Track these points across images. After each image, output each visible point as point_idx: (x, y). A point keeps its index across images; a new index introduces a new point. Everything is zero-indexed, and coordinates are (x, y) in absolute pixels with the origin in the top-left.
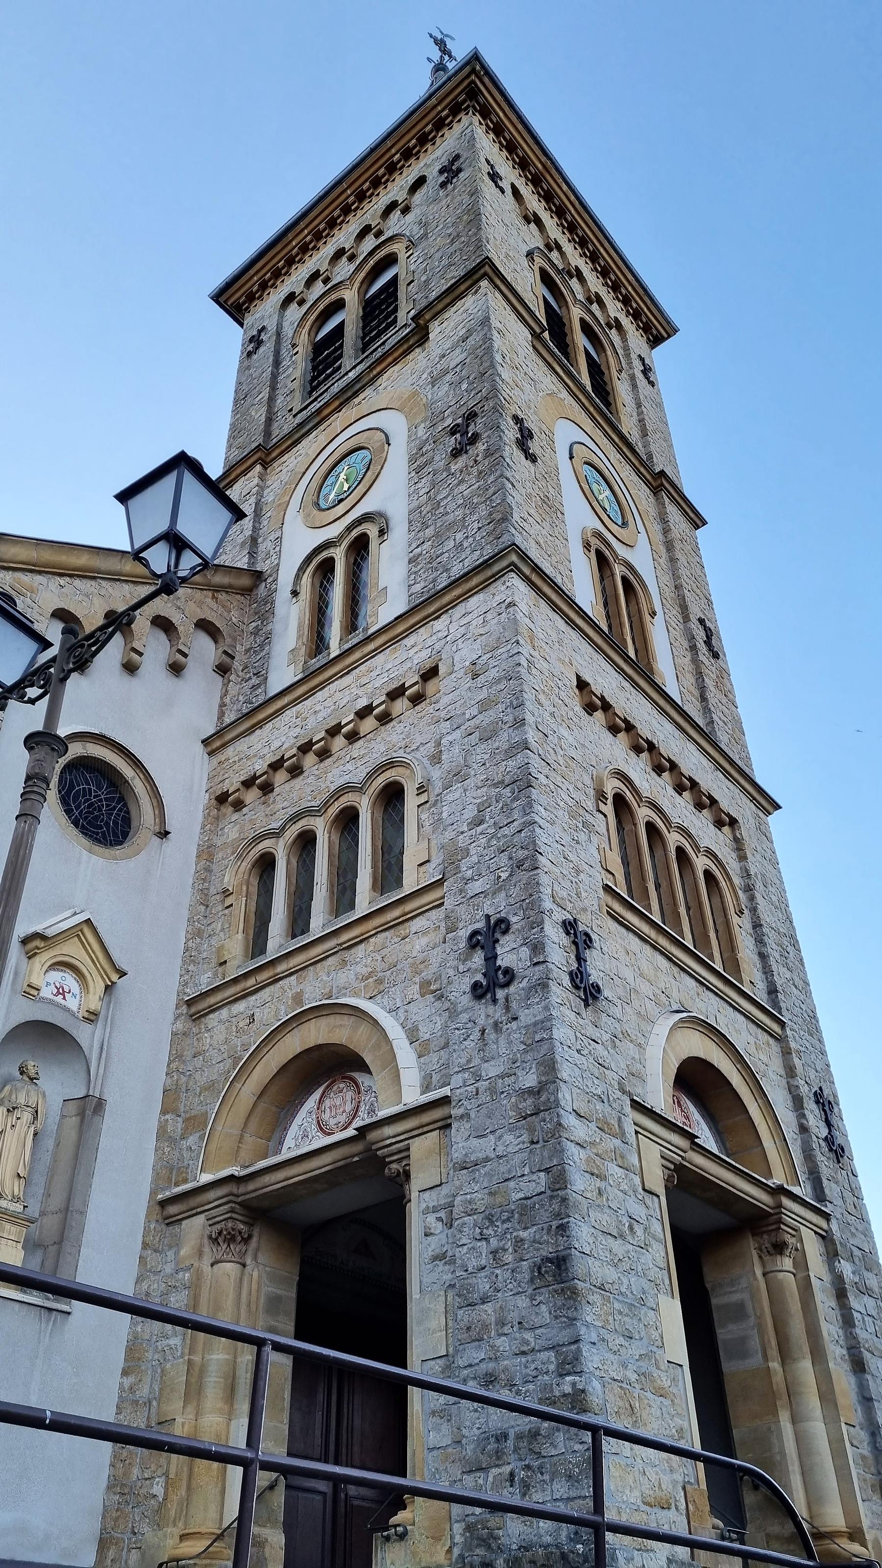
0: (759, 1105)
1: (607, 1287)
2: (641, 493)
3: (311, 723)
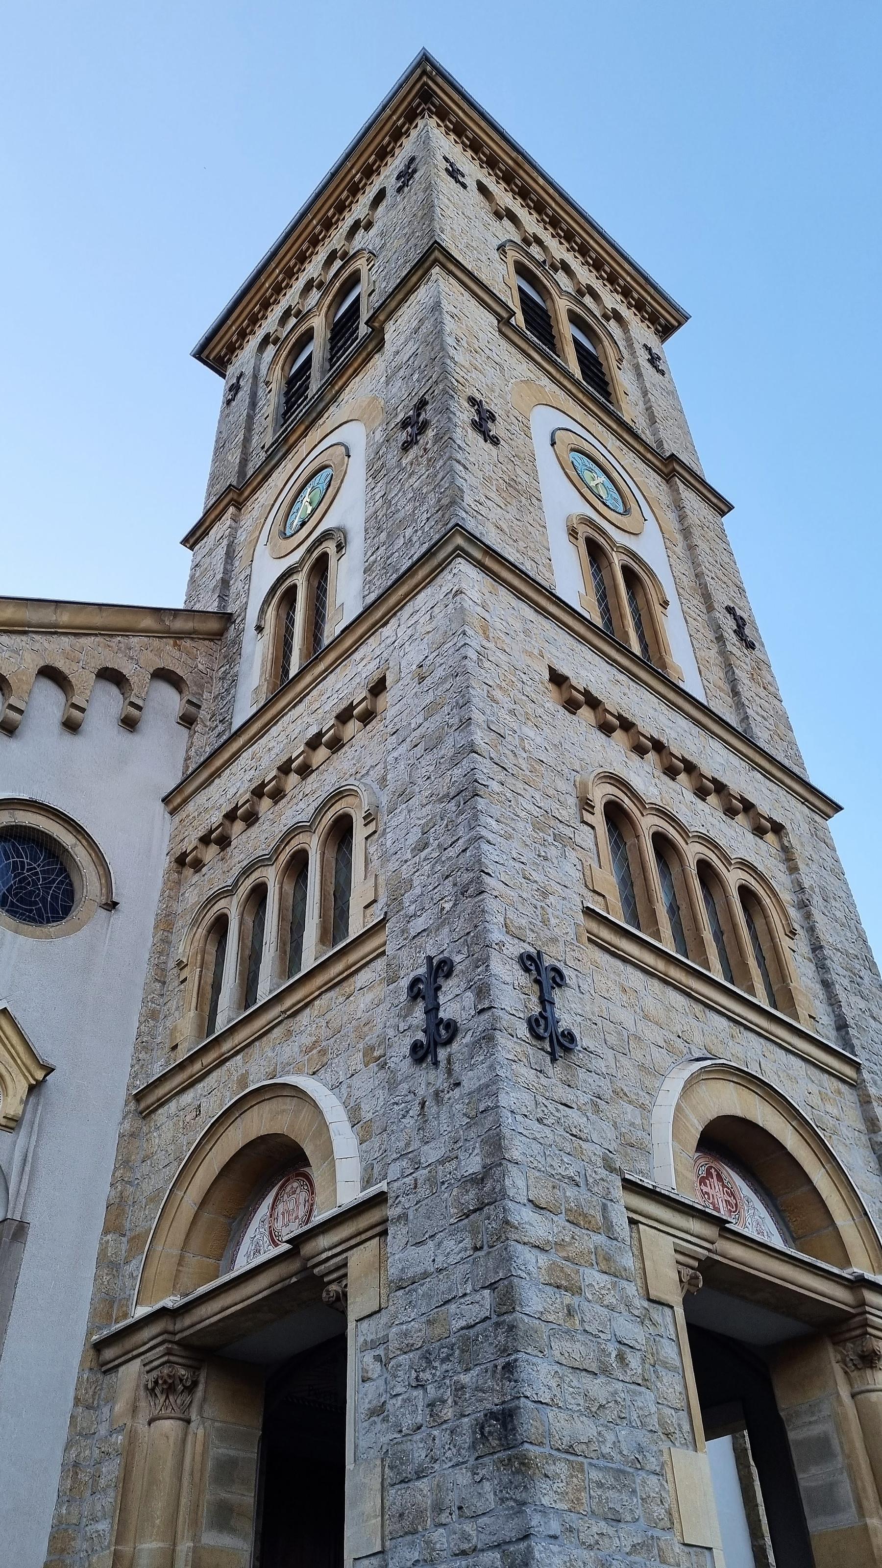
0: (827, 1171)
1: (578, 1449)
2: (651, 481)
3: (265, 762)
